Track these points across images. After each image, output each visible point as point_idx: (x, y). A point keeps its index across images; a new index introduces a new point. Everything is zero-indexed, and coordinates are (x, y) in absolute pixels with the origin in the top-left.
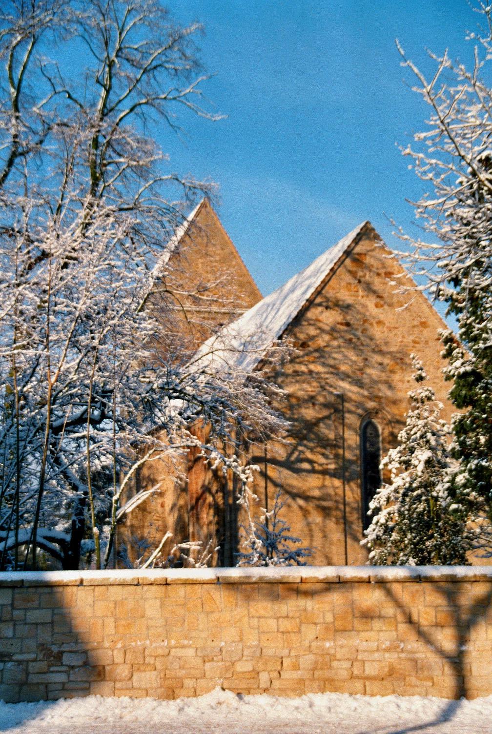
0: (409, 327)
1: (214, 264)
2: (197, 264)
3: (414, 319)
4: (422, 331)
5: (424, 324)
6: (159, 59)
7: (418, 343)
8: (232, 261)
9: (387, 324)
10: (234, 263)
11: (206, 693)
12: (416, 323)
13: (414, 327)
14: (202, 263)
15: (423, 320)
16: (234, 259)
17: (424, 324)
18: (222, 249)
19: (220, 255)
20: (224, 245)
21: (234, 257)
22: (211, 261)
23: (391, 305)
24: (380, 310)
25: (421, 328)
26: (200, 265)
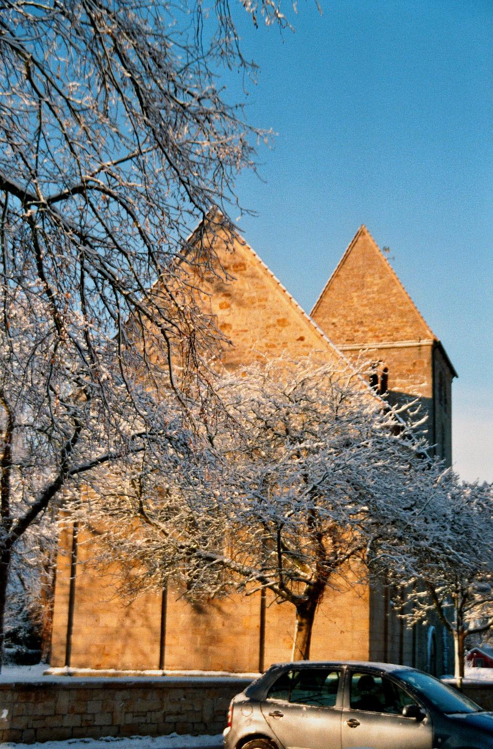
0: (262, 328)
1: (371, 296)
2: (352, 298)
3: (269, 318)
4: (280, 331)
5: (282, 322)
6: (143, 49)
7: (274, 346)
8: (392, 290)
9: (234, 328)
10: (394, 291)
11: (180, 733)
12: (271, 322)
13: (268, 327)
14: (358, 296)
15: (281, 317)
16: (395, 287)
17: (282, 322)
18: (381, 278)
19: (378, 284)
20: (383, 273)
21: (395, 284)
22: (368, 293)
23: (240, 304)
24: (226, 312)
25: (280, 328)
26: (355, 299)
